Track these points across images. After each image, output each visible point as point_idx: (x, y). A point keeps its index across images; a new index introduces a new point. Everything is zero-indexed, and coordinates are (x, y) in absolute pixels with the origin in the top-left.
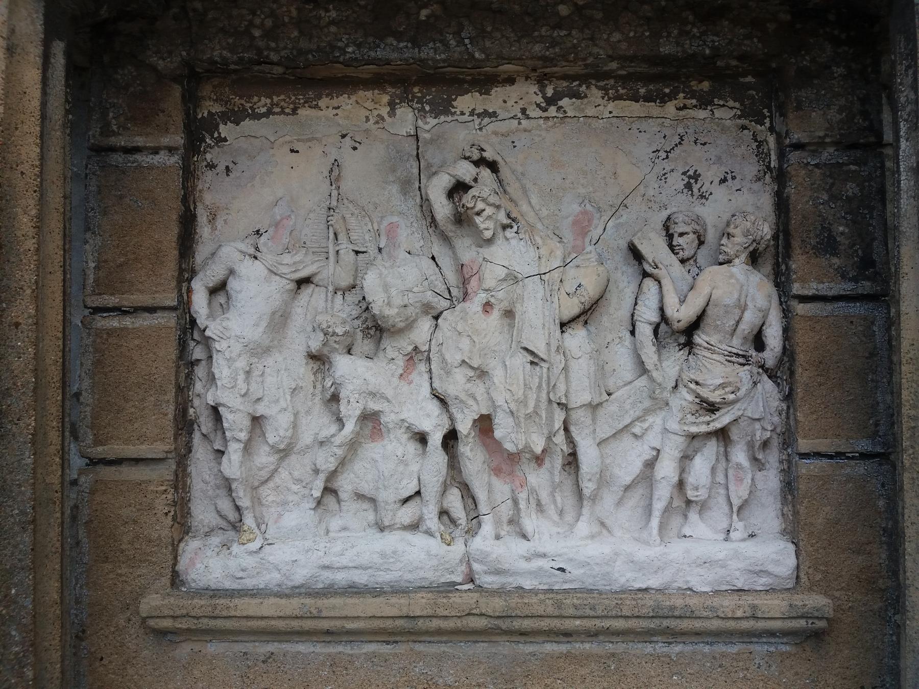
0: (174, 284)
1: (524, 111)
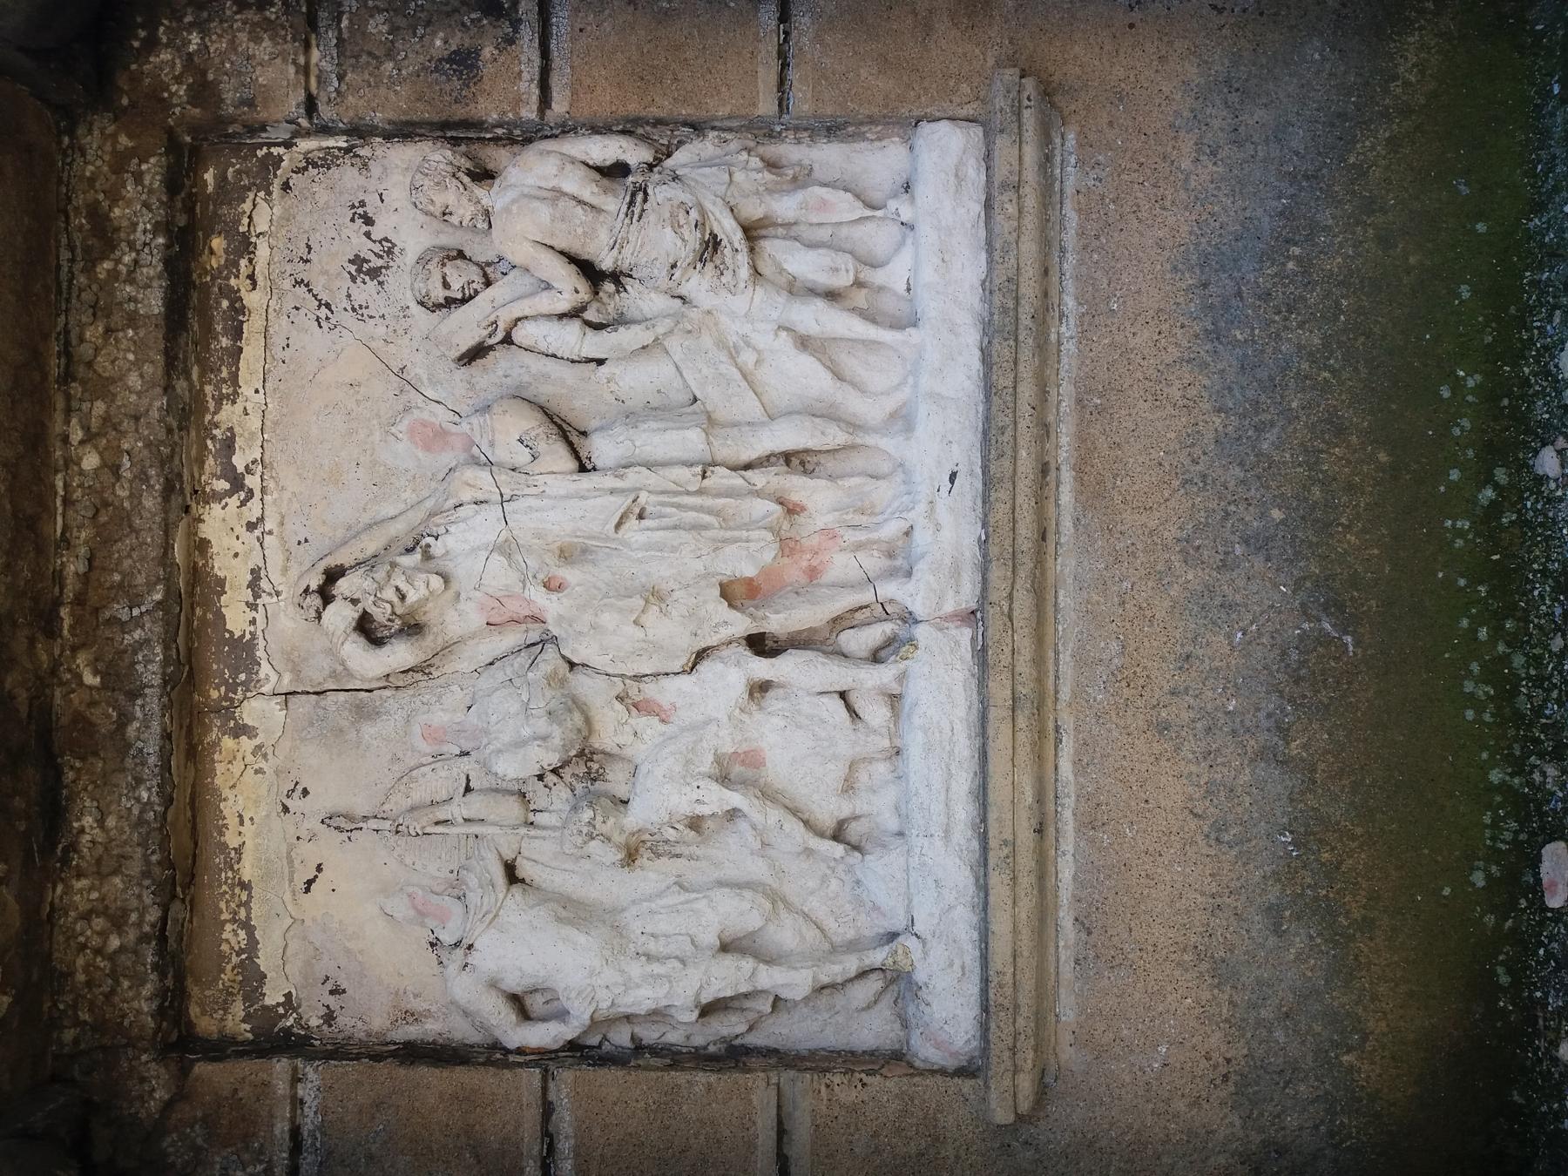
0: (507, 1074)
1: (251, 526)
